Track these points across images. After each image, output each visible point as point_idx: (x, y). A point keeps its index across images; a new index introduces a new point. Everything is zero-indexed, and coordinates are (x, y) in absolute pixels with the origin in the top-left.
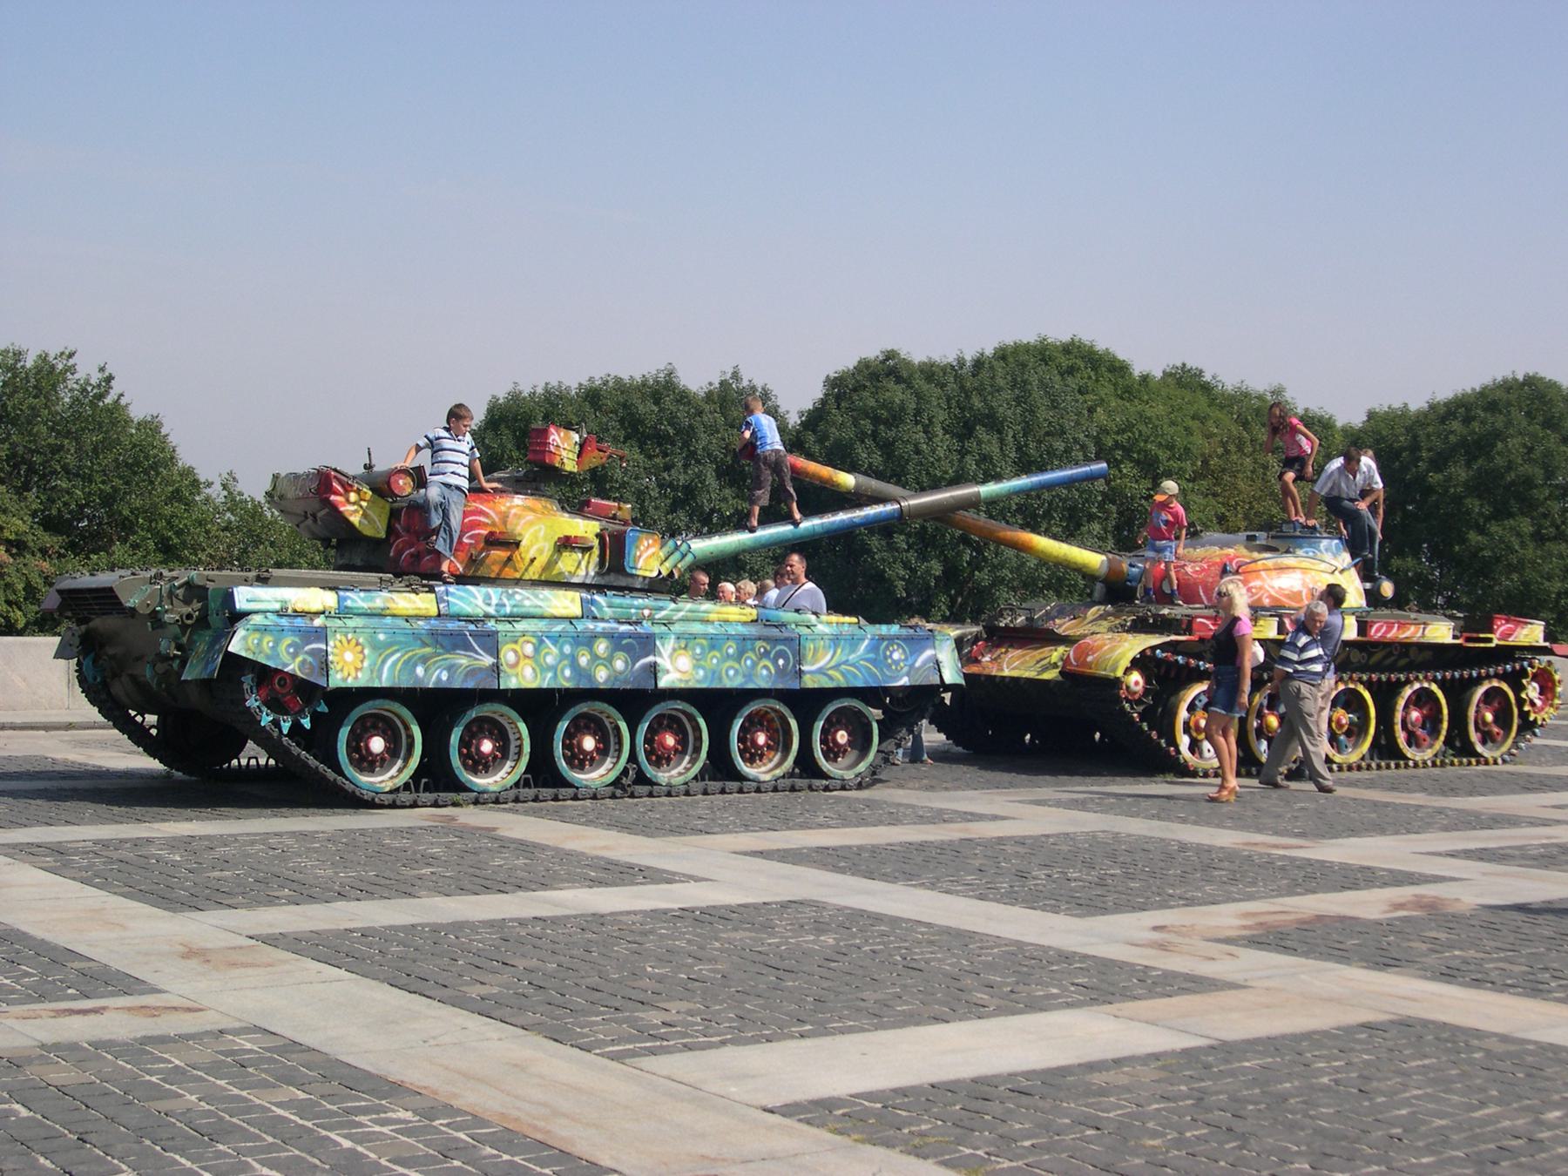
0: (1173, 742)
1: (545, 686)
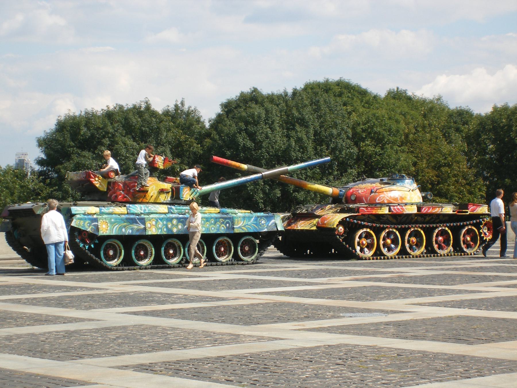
0: (354, 248)
1: (159, 234)
